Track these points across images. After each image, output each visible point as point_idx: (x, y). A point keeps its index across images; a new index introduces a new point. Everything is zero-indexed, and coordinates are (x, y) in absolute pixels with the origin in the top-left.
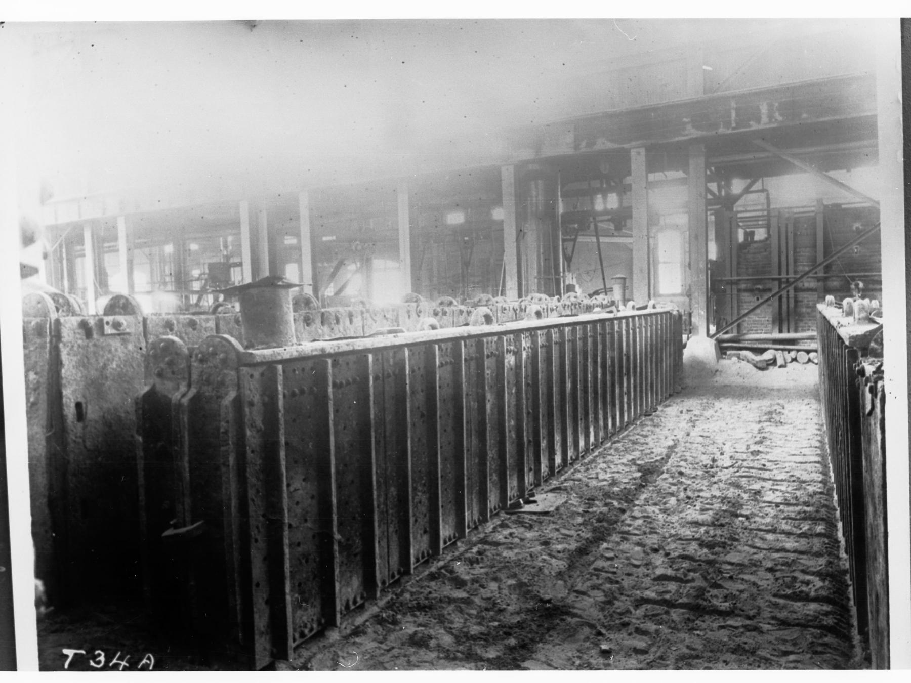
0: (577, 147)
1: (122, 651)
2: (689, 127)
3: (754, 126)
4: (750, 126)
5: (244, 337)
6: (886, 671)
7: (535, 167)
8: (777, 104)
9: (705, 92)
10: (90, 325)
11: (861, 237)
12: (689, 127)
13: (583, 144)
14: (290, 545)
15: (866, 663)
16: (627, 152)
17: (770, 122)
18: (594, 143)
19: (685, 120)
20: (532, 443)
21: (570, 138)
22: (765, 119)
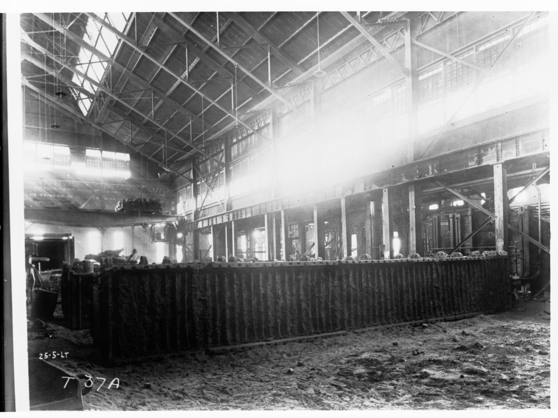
0: (365, 189)
1: (63, 388)
2: (403, 178)
3: (427, 176)
4: (425, 176)
5: (416, 308)
6: (28, 406)
7: (368, 195)
8: (435, 165)
9: (415, 160)
10: (124, 254)
11: (413, 292)
12: (403, 178)
13: (368, 188)
14: (133, 49)
15: (31, 404)
16: (381, 190)
17: (433, 174)
18: (371, 187)
19: (402, 175)
20: (81, 147)
21: (362, 186)
22: (431, 173)
